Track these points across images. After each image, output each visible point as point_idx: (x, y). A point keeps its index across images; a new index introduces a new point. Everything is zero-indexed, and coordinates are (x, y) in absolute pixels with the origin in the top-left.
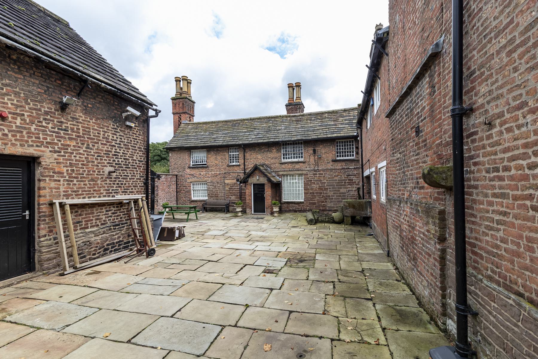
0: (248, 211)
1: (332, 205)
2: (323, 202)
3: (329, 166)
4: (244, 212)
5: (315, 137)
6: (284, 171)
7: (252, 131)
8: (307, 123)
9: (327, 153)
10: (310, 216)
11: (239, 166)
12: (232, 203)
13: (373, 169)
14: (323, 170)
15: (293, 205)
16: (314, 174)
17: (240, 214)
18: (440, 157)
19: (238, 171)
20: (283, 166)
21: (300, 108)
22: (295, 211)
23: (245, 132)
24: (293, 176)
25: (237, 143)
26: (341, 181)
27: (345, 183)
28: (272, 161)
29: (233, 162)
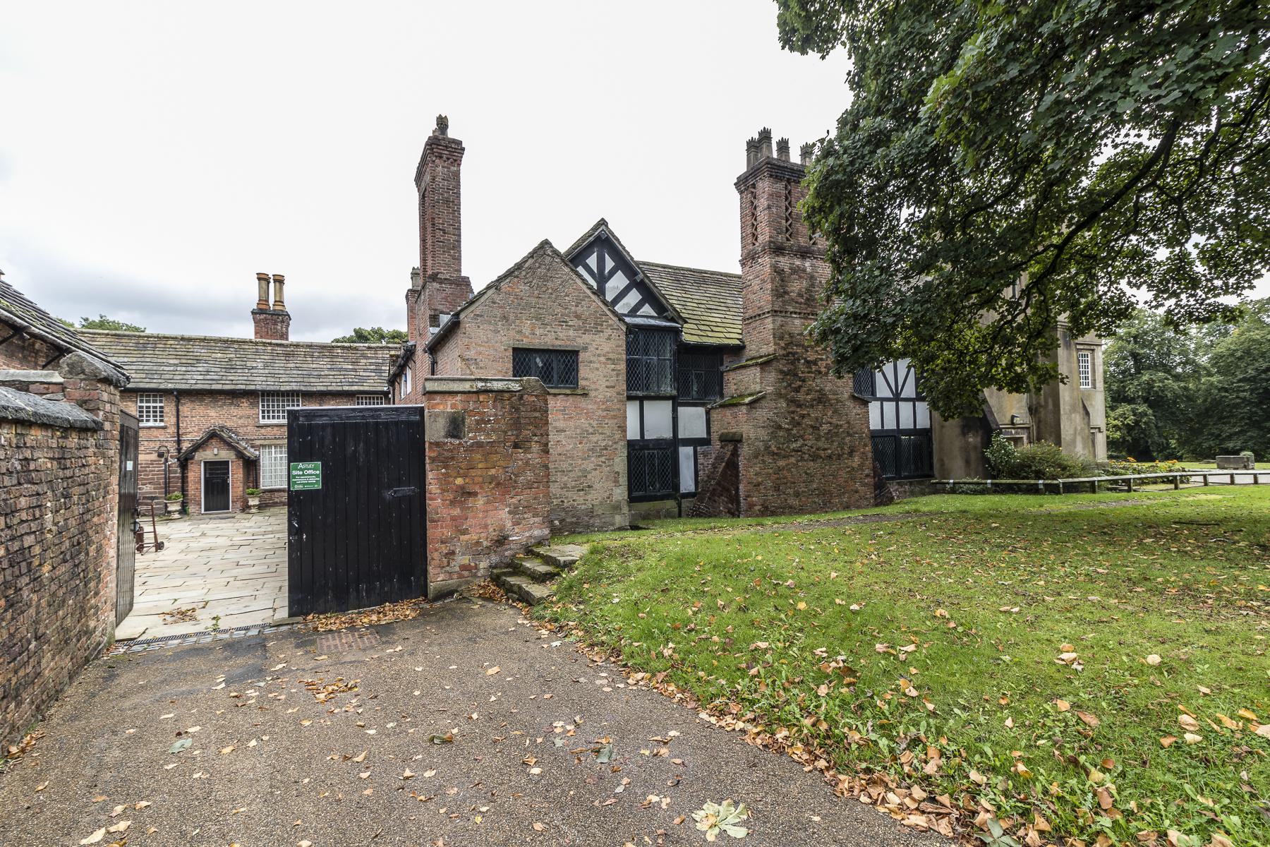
0: (192, 509)
4: (184, 511)
7: (192, 365)
8: (305, 362)
11: (164, 428)
17: (177, 516)
19: (162, 438)
20: (263, 431)
21: (283, 322)
23: (176, 365)
25: (162, 387)
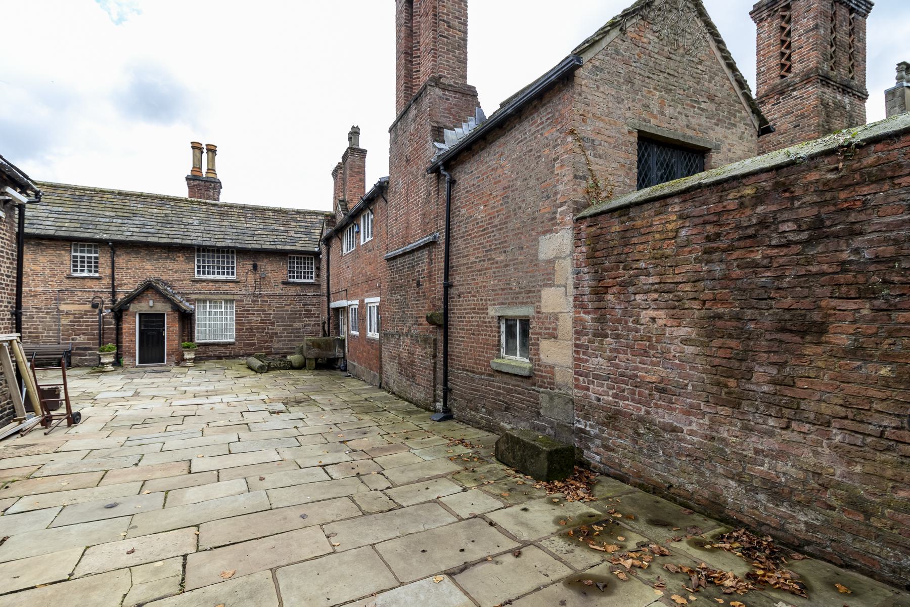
0: (125, 361)
1: (280, 345)
2: (267, 342)
3: (278, 290)
4: (117, 363)
5: (257, 246)
6: (200, 294)
7: (128, 218)
9: (275, 272)
10: (257, 363)
12: (78, 349)
13: (355, 303)
14: (269, 296)
15: (216, 348)
16: (252, 301)
17: (110, 368)
18: (434, 306)
19: (96, 289)
20: (198, 285)
21: (214, 188)
22: (219, 358)
23: (112, 217)
24: (215, 302)
25: (97, 236)
26: (294, 312)
27: (300, 314)
28: (176, 276)
29: (82, 271)
